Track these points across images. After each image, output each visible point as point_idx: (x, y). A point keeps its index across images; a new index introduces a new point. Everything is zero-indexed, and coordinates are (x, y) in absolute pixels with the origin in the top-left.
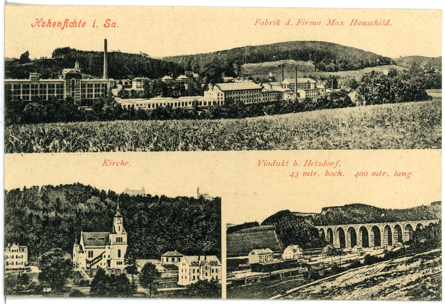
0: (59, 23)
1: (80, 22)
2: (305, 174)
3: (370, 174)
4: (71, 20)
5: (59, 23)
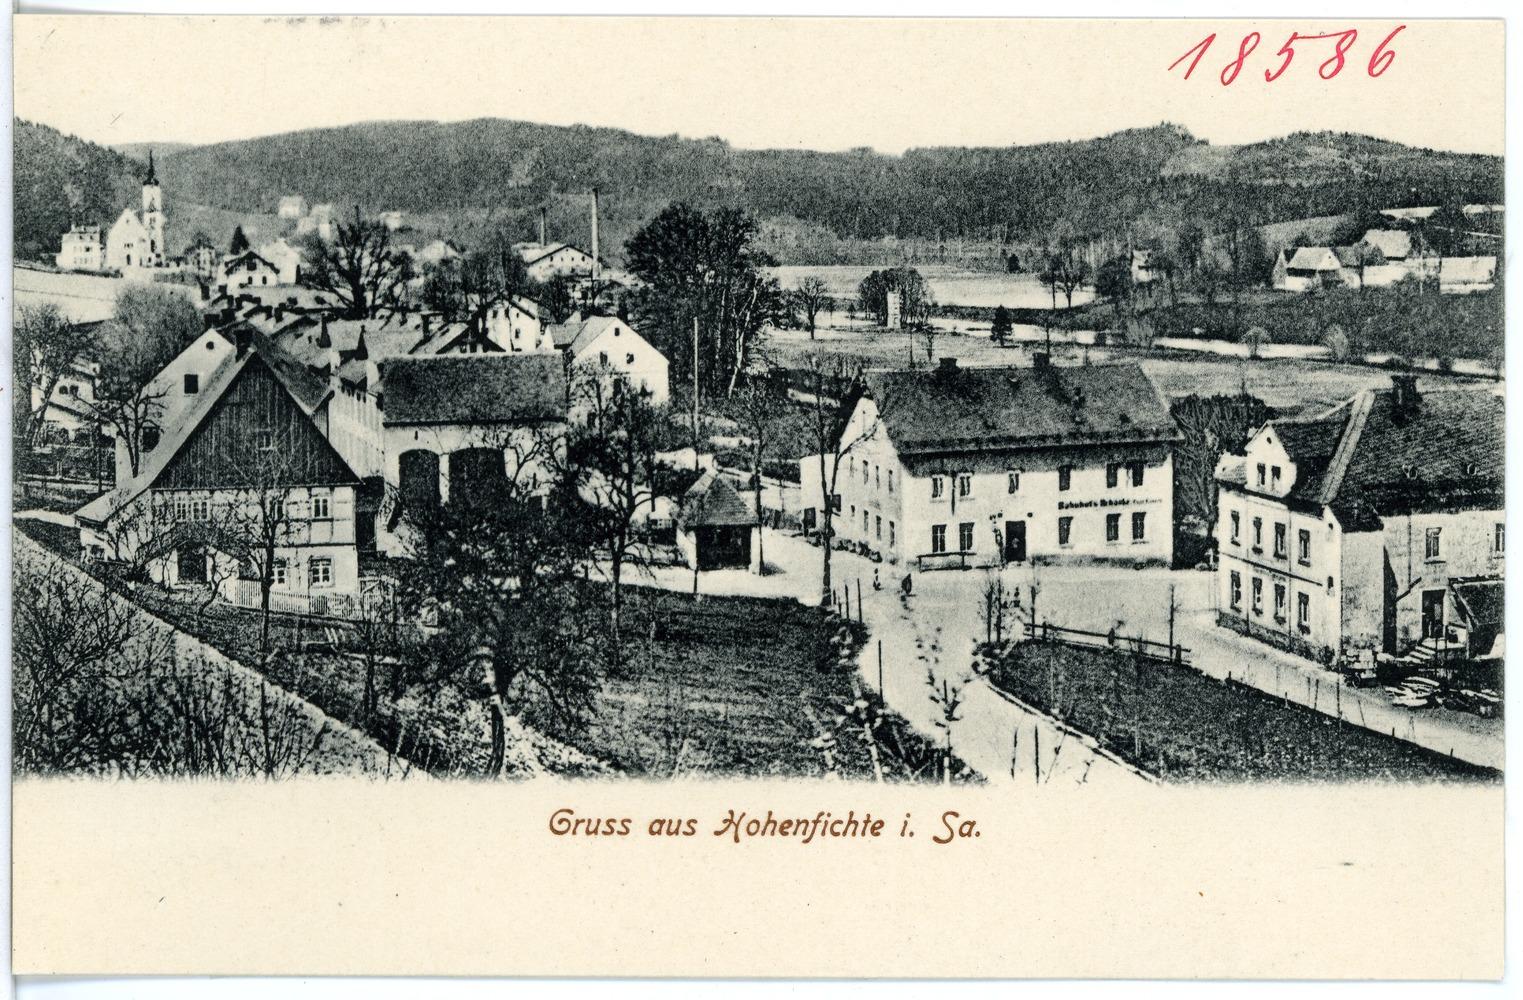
0: (799, 823)
1: (867, 822)
2: (657, 827)
3: (639, 828)
4: (779, 818)
5: (799, 823)
